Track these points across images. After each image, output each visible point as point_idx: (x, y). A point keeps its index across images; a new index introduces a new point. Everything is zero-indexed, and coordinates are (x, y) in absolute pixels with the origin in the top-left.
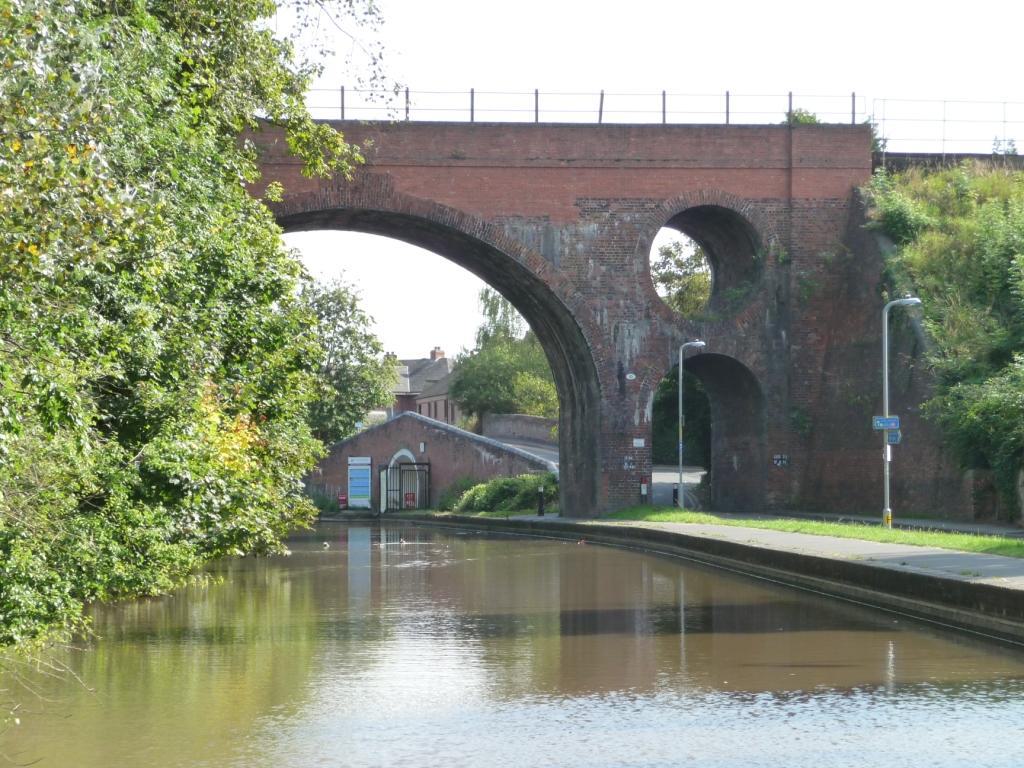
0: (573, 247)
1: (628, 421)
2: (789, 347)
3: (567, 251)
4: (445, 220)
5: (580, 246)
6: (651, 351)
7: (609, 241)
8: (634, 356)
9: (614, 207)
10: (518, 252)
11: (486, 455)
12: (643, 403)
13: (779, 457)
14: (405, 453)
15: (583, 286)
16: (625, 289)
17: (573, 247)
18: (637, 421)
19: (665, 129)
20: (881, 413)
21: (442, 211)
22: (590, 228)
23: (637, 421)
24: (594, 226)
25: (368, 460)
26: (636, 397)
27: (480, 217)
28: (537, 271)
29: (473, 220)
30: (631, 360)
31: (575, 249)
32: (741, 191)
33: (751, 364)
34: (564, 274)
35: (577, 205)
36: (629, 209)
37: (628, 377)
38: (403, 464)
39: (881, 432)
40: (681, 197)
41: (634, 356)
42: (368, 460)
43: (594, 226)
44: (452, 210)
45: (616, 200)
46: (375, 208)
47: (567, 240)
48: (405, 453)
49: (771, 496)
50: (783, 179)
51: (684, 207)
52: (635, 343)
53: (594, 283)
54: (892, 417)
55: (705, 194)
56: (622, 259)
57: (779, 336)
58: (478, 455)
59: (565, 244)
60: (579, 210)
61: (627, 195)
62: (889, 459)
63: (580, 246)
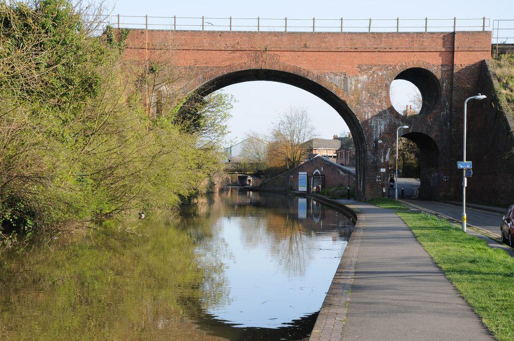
0: (356, 86)
1: (378, 161)
2: (451, 130)
3: (353, 87)
4: (301, 74)
5: (359, 85)
6: (389, 131)
7: (372, 83)
8: (382, 133)
9: (374, 68)
10: (332, 88)
11: (342, 173)
12: (385, 153)
13: (445, 177)
14: (317, 171)
15: (359, 102)
16: (378, 104)
17: (356, 86)
18: (382, 161)
19: (399, 34)
20: (462, 160)
21: (300, 71)
22: (364, 78)
23: (382, 161)
24: (365, 77)
25: (306, 173)
26: (382, 151)
27: (315, 72)
28: (340, 96)
29: (313, 74)
30: (380, 135)
31: (357, 87)
32: (433, 63)
33: (434, 137)
34: (352, 97)
35: (358, 67)
36: (381, 70)
37: (379, 142)
38: (317, 174)
39: (462, 170)
40: (404, 64)
41: (382, 133)
42: (306, 173)
43: (365, 77)
44: (304, 70)
45: (375, 65)
46: (271, 69)
47: (353, 83)
48: (317, 171)
49: (441, 194)
50: (450, 56)
51: (405, 69)
52: (383, 127)
53: (365, 101)
54: (467, 162)
55: (415, 63)
56: (378, 91)
57: (446, 125)
58: (339, 172)
59: (354, 86)
60: (359, 69)
61: (380, 63)
62: (466, 185)
63: (359, 85)
